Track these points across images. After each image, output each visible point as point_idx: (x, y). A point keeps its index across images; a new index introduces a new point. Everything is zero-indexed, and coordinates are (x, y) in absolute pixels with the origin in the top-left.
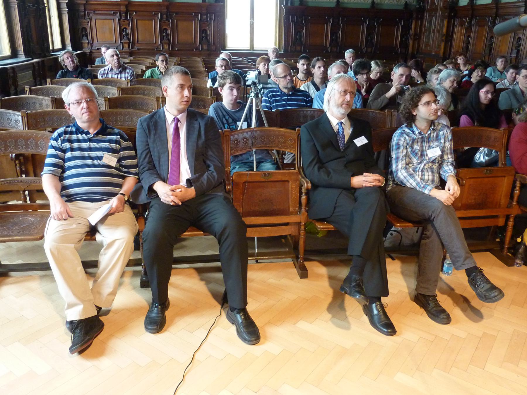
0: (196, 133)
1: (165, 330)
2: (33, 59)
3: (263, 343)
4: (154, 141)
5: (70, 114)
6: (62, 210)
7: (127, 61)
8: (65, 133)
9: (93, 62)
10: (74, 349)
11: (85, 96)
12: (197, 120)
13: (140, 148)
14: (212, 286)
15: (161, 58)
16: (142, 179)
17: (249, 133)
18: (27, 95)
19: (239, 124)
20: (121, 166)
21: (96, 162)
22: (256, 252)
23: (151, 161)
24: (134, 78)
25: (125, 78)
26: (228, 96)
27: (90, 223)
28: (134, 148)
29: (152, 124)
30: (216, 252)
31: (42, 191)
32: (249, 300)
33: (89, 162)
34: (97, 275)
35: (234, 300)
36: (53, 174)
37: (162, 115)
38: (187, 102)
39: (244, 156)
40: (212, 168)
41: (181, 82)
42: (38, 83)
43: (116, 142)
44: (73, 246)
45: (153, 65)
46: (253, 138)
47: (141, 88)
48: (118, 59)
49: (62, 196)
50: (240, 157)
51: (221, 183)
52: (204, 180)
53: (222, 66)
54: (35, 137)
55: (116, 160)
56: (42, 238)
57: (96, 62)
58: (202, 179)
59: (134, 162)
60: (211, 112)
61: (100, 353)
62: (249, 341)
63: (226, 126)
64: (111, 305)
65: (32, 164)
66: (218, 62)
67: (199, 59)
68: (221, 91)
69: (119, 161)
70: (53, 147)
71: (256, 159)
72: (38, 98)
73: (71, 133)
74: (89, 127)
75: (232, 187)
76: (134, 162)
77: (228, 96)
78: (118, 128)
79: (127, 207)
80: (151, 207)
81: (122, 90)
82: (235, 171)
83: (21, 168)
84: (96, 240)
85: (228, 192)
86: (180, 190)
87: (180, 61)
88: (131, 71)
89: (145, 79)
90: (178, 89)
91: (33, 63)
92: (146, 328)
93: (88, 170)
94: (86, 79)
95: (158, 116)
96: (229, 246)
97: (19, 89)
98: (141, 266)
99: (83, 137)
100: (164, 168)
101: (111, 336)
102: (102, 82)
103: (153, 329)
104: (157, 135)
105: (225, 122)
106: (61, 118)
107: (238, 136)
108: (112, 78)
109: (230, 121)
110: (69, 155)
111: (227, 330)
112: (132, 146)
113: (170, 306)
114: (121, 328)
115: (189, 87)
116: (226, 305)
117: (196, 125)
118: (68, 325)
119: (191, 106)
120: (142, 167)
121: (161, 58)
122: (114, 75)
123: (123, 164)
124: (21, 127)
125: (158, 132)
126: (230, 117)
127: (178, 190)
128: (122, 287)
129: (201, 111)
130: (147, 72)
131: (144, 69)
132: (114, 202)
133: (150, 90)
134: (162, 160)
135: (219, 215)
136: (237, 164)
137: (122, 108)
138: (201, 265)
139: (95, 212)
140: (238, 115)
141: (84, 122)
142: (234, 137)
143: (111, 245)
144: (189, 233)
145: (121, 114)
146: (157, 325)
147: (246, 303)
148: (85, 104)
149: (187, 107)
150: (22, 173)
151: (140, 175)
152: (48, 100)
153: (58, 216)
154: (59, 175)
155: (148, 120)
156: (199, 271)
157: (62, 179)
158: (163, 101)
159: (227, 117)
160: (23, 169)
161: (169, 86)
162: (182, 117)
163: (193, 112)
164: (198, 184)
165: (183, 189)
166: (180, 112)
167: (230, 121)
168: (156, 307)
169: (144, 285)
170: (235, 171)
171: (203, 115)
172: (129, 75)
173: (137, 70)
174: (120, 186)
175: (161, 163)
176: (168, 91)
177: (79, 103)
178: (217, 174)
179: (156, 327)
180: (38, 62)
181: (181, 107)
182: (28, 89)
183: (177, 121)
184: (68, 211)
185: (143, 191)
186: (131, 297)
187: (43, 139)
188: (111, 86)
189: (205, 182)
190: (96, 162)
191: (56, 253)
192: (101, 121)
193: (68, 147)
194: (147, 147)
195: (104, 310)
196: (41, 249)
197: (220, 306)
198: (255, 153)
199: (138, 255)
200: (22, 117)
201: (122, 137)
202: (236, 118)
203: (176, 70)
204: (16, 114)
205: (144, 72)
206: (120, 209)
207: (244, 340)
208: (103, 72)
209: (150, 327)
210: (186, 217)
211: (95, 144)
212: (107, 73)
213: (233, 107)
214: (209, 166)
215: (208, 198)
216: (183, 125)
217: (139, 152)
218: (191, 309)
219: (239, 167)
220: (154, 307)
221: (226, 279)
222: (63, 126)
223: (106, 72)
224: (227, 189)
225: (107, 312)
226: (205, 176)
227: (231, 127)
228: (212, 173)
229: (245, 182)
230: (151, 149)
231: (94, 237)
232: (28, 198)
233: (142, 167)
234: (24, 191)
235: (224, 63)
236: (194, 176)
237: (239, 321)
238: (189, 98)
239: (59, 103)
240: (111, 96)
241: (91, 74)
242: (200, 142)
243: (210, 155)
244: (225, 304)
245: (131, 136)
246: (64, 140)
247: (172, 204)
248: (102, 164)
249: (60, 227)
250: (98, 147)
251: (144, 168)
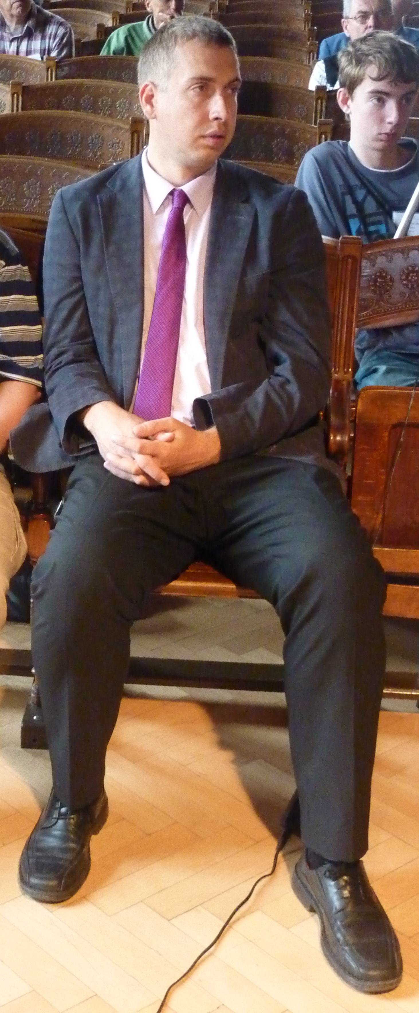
0: (242, 243)
1: (84, 898)
4: (100, 267)
12: (247, 200)
13: (55, 286)
16: (52, 391)
23: (85, 334)
24: (69, 55)
28: (36, 287)
29: (96, 210)
30: (270, 656)
32: (375, 836)
35: (323, 829)
38: (218, 137)
40: (285, 369)
41: (203, 70)
47: (88, 88)
51: (314, 422)
52: (256, 404)
53: (364, 16)
59: (32, 332)
60: (306, 176)
62: (360, 978)
63: (355, 224)
68: (345, 101)
76: (32, 332)
80: (72, 485)
81: (28, 94)
82: (370, 382)
85: (336, 455)
86: (167, 435)
88: (61, 31)
89: (106, 60)
90: (191, 93)
92: (24, 881)
95: (118, 183)
96: (318, 642)
98: (29, 674)
100: (124, 357)
103: (46, 889)
104: (112, 248)
105: (351, 209)
107: (390, 260)
109: (370, 206)
111: (286, 930)
112: (28, 277)
113: (110, 820)
115: (229, 86)
117: (244, 219)
119: (226, 154)
120: (54, 352)
125: (116, 236)
126: (369, 192)
127: (163, 437)
129: (273, 169)
130: (114, 34)
133: (115, 95)
134: (121, 330)
135: (294, 534)
136: (381, 360)
137: (21, 152)
138: (229, 696)
140: (396, 186)
142: (373, 263)
144: (190, 584)
146: (59, 878)
147: (362, 846)
149: (215, 155)
151: (46, 377)
155: (86, 194)
156: (219, 715)
158: (139, 131)
159: (360, 194)
161: (161, 82)
162: (197, 189)
163: (240, 169)
164: (232, 419)
165: (179, 435)
166: (194, 171)
167: (370, 206)
169: (33, 738)
170: (370, 382)
172: (54, 44)
173: (82, 28)
175: (116, 341)
176: (160, 100)
179: (53, 883)
181: (197, 155)
183: (182, 200)
185: (52, 430)
189: (257, 415)
194: (76, 286)
197: (273, 844)
203: (189, 30)
207: (344, 970)
209: (34, 881)
210: (184, 530)
214: (277, 361)
215: (277, 466)
216: (200, 218)
217: (50, 300)
218: (176, 838)
219: (388, 372)
220: (56, 815)
221: (299, 759)
226: (259, 395)
227: (372, 229)
228: (283, 385)
229: (399, 426)
230: (89, 292)
233: (54, 352)
236: (223, 392)
237: (330, 903)
238: (225, 124)
242: (252, 278)
243: (284, 323)
244: (293, 837)
247: (138, 480)
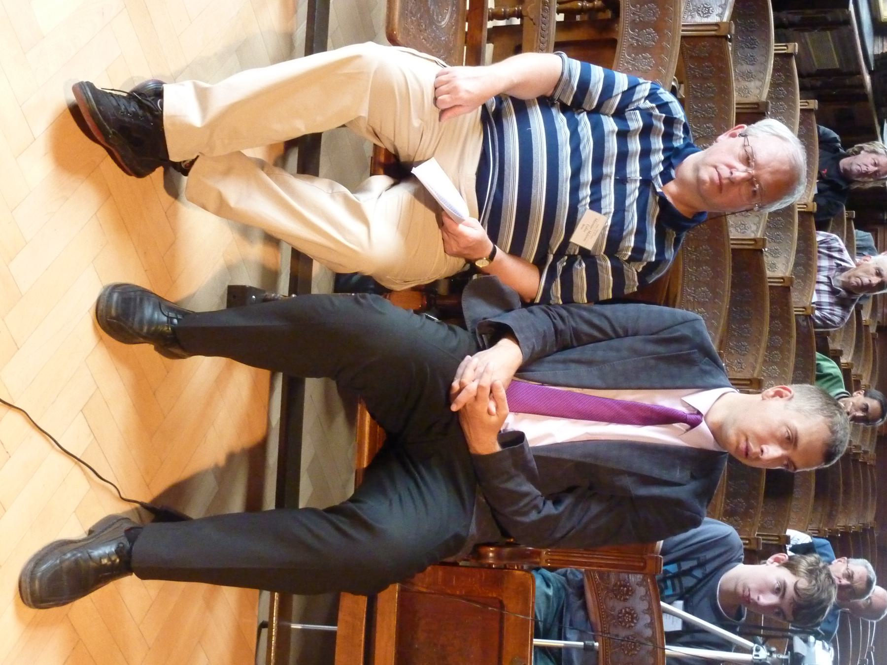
1: (101, 339)
2: (871, 73)
3: (19, 615)
4: (635, 352)
5: (720, 138)
6: (463, 95)
7: (866, 317)
8: (670, 121)
9: (861, 225)
10: (85, 94)
11: (766, 177)
12: (693, 477)
13: (620, 314)
14: (209, 486)
15: (874, 404)
16: (531, 312)
17: (648, 632)
18: (774, 47)
19: (677, 607)
20: (572, 260)
21: (585, 193)
22: (294, 626)
23: (579, 339)
25: (819, 304)
26: (760, 579)
27: (420, 163)
28: (619, 298)
29: (685, 349)
30: (306, 495)
31: (518, 50)
32: (154, 586)
33: (587, 176)
34: (277, 171)
35: (159, 541)
36: (561, 82)
37: (713, 381)
39: (581, 614)
40: (549, 509)
41: (803, 440)
42: (807, 81)
43: (639, 251)
44: (364, 113)
45: (852, 384)
46: (634, 642)
48: (869, 287)
49: (500, 99)
50: (576, 603)
51: (505, 534)
52: (520, 485)
53: (850, 577)
54: (663, 48)
55: (589, 246)
56: (393, 41)
57: (862, 233)
58: (521, 479)
59: (581, 295)
60: (714, 527)
61: (64, 160)
63: (672, 568)
64: (191, 199)
65: (592, 37)
66: (861, 567)
67: (870, 518)
69: (584, 253)
70: (632, 89)
71: (568, 649)
72: (765, 69)
73: (668, 136)
74: (682, 183)
75: (490, 566)
76: (581, 295)
77: (760, 579)
78: (676, 259)
79: (455, 265)
80: (451, 329)
81: (783, 291)
82: (539, 582)
83: (581, 11)
84: (372, 175)
85: (477, 553)
86: (493, 410)
87: (864, 464)
88: (837, 319)
89: (812, 358)
90: (784, 430)
91: (859, 72)
92: (115, 287)
93: (566, 171)
94: (814, 200)
95: (708, 368)
97: (790, 32)
98: (290, 294)
99: (657, 165)
100: (560, 373)
101: (107, 193)
102: (806, 240)
104: (652, 362)
105: (686, 565)
106: (710, 120)
107: (642, 599)
108: (819, 269)
109: (688, 582)
110: (610, 125)
111: (76, 512)
112: (627, 291)
114: (124, 222)
115: (789, 461)
116: (147, 516)
117: (677, 475)
118: (152, 86)
119: (732, 460)
120: (564, 313)
121: (874, 404)
122: (826, 273)
123: (576, 265)
124: (690, 20)
125: (662, 366)
126: (700, 581)
127: (492, 406)
128: (237, 236)
130: (834, 364)
131: (843, 360)
132: (473, 229)
133: (782, 365)
134: (583, 370)
135: (409, 517)
136: (557, 591)
137: (734, 285)
139: (449, 178)
140: (705, 604)
141: (697, 169)
143: (357, 212)
144: (367, 429)
145: (718, 275)
146: (117, 318)
147: (144, 575)
148: (743, 175)
150: (570, 14)
151: (543, 307)
152: (761, 93)
153: (447, 82)
154: (556, 97)
156: (256, 455)
157: (546, 102)
159: (698, 573)
160: (578, 18)
161: (793, 404)
162: (702, 434)
164: (508, 464)
165: (494, 419)
166: (718, 432)
167: (688, 582)
168: (170, 319)
170: (539, 582)
171: (706, 495)
173: (839, 337)
174: (516, 251)
175: (573, 366)
176: (778, 403)
177: (747, 160)
178: (534, 522)
179: (113, 312)
180: (862, 85)
181: (731, 434)
182: (790, 51)
183: (693, 421)
184: (457, 110)
185: (497, 311)
186: (207, 253)
187: (657, 65)
188: (796, 265)
189: (510, 485)
190: (585, 193)
191: (349, 70)
192: (698, 215)
193: (630, 123)
194: (621, 332)
195: (179, 181)
196: (362, 32)
197: (147, 499)
198: (587, 648)
199: (320, 283)
200: (717, 24)
201: (651, 268)
202: (696, 599)
204: (724, 9)
205: (836, 356)
206: (453, 243)
207: (39, 559)
208: (836, 245)
209: (115, 296)
210: (414, 423)
211: (637, 193)
212: (831, 257)
213: (725, 587)
214: (557, 502)
215: (466, 495)
216: (678, 437)
217: (608, 310)
218: (151, 417)
219: (547, 597)
220: (171, 315)
222: (687, 115)
223: (836, 254)
224: (483, 550)
225: (173, 190)
226: (528, 487)
227: (669, 583)
228: (536, 507)
229: (502, 606)
230: (615, 343)
231: (381, 171)
232: (502, 23)
233: (564, 313)
234: (519, 15)
235: (860, 585)
236: (530, 457)
237: (96, 547)
238: (758, 459)
239: (752, 114)
240: (768, 259)
241: (830, 214)
243: (589, 508)
244: (153, 516)
245: (651, 292)
246: (651, 115)
247: (456, 385)
248: (580, 209)
249: (417, 87)
250: (627, 203)
251: (562, 318)
